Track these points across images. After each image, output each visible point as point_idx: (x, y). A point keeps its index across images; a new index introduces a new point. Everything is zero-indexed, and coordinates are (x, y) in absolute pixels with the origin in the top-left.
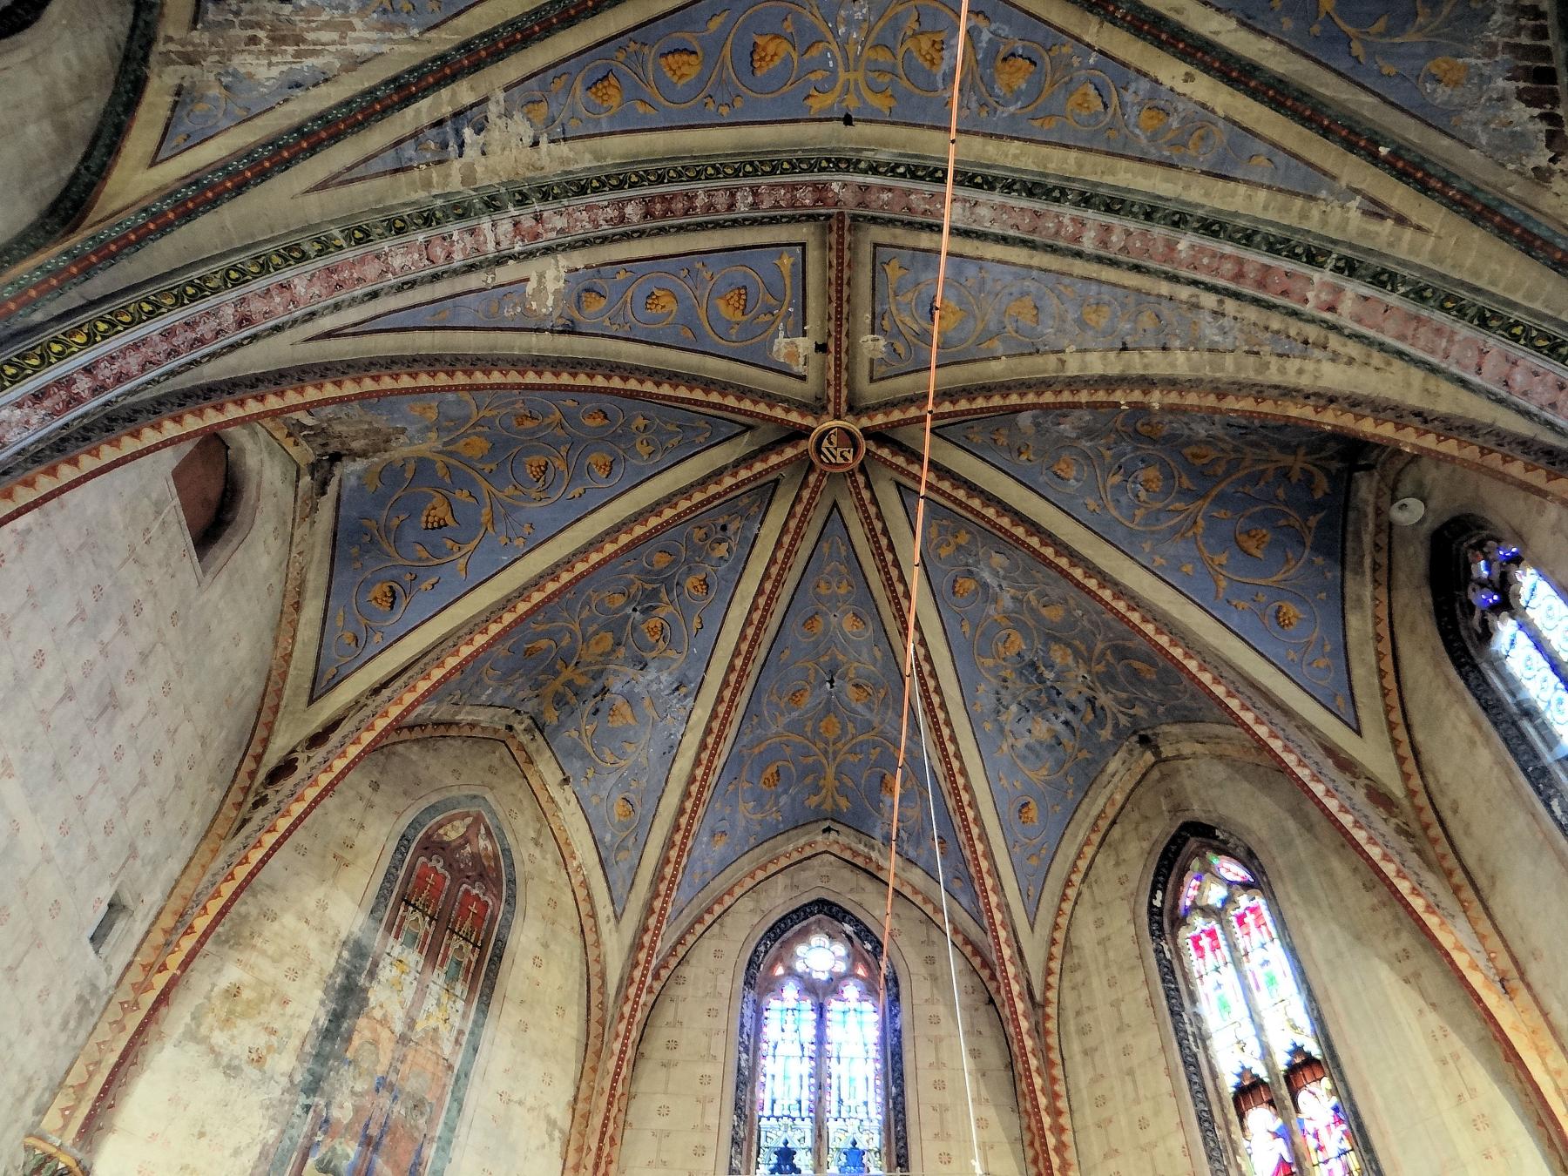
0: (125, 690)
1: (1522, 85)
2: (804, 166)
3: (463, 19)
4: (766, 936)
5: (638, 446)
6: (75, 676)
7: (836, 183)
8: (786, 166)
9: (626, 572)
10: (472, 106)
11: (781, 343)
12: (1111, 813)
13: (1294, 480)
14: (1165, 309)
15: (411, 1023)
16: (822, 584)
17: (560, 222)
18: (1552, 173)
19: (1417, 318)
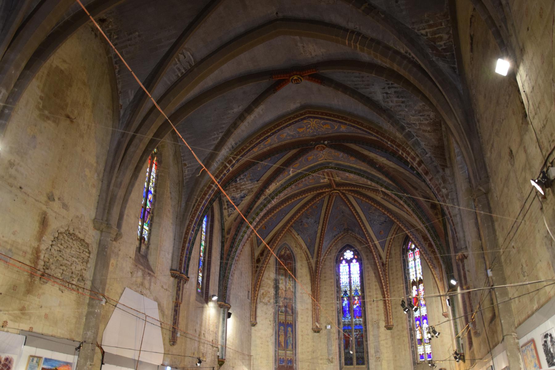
15: (286, 288)
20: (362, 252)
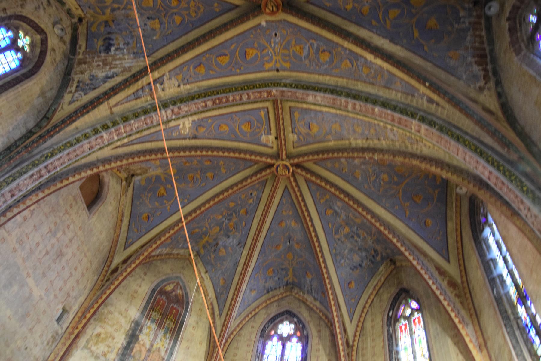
0: (65, 250)
4: (269, 321)
6: (49, 248)
10: (159, 78)
11: (264, 137)
12: (380, 284)
13: (430, 178)
14: (377, 128)
15: (152, 346)
17: (186, 109)
18: (484, 88)
20: (311, 325)
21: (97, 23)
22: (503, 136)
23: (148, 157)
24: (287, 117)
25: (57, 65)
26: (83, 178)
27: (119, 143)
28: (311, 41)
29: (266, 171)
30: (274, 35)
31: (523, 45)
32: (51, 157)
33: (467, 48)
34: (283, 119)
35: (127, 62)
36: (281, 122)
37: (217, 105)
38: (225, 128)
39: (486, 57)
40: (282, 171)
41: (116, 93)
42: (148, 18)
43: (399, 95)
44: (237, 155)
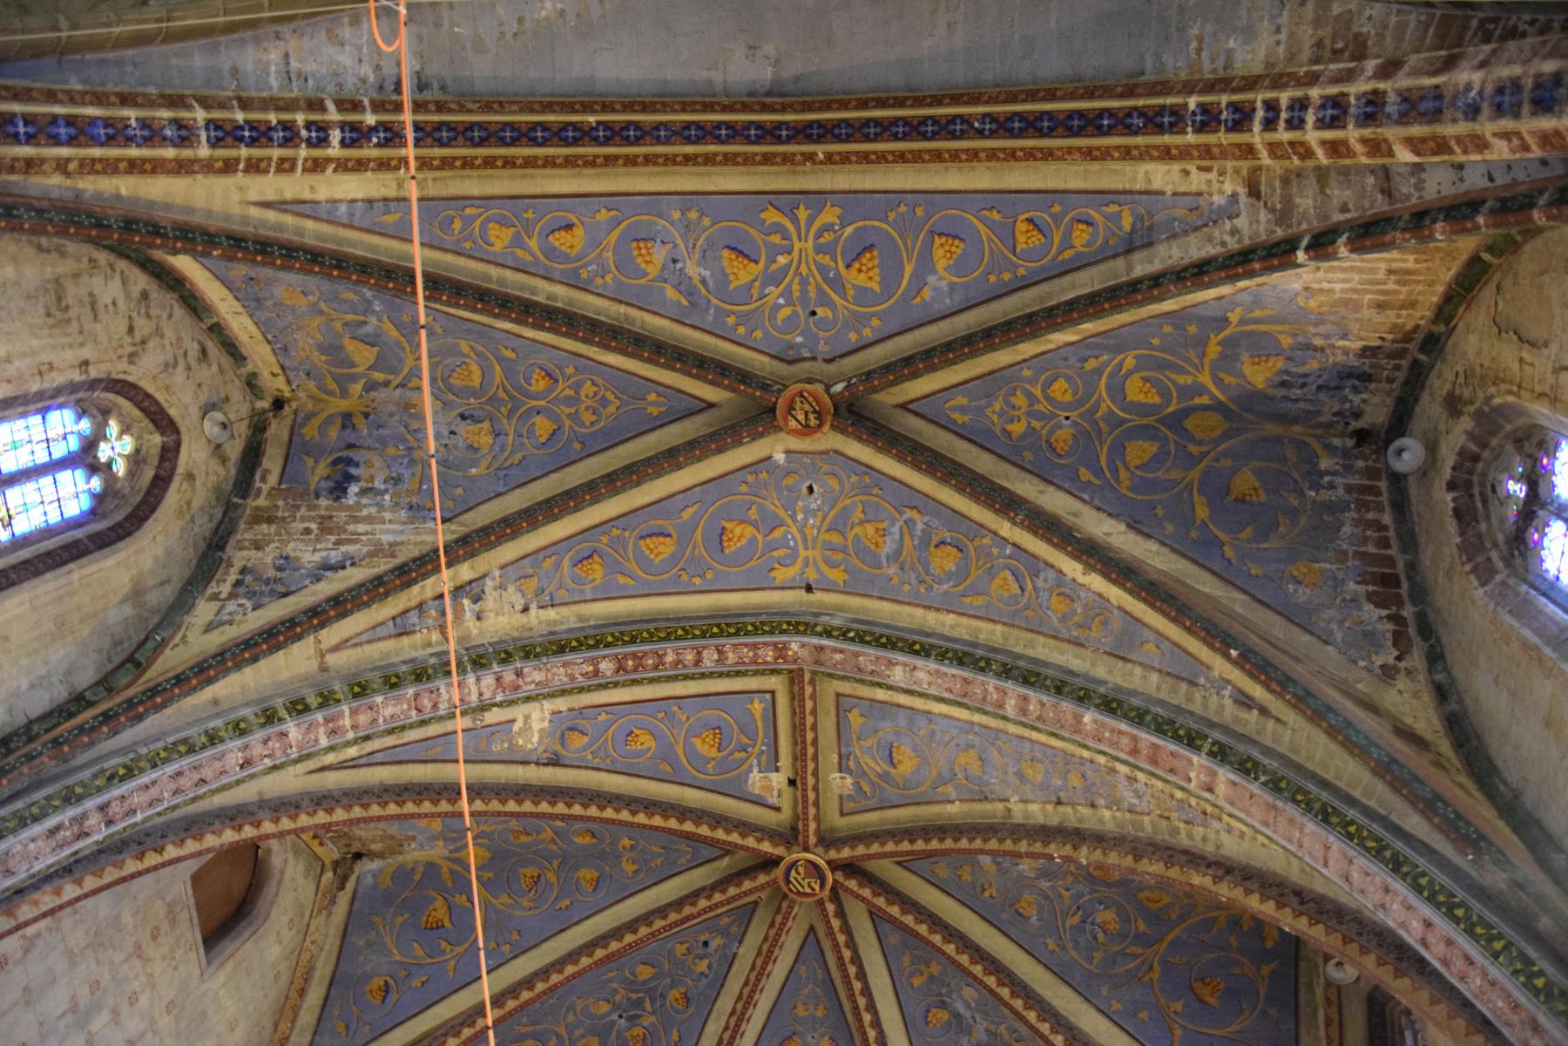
1: (1371, 588)
2: (767, 628)
3: (471, 514)
5: (624, 864)
7: (795, 645)
8: (750, 628)
9: (610, 980)
10: (471, 582)
11: (755, 777)
13: (1245, 928)
16: (799, 1005)
17: (538, 676)
18: (1398, 671)
19: (1274, 807)
21: (325, 414)
22: (1459, 816)
23: (410, 808)
24: (828, 724)
25: (192, 520)
26: (208, 851)
27: (330, 758)
28: (909, 514)
29: (754, 879)
30: (805, 490)
31: (1494, 555)
32: (123, 779)
33: (1342, 557)
34: (814, 727)
35: (386, 529)
36: (810, 736)
37: (627, 674)
38: (646, 741)
39: (1398, 585)
40: (802, 882)
41: (344, 615)
42: (463, 417)
43: (1154, 677)
44: (673, 823)
